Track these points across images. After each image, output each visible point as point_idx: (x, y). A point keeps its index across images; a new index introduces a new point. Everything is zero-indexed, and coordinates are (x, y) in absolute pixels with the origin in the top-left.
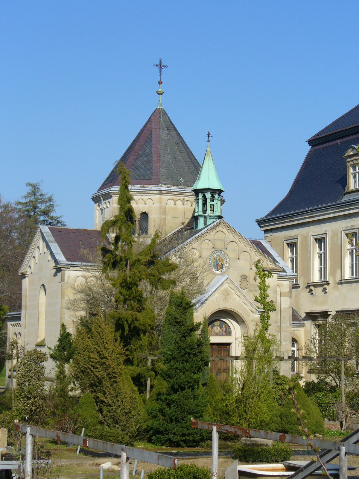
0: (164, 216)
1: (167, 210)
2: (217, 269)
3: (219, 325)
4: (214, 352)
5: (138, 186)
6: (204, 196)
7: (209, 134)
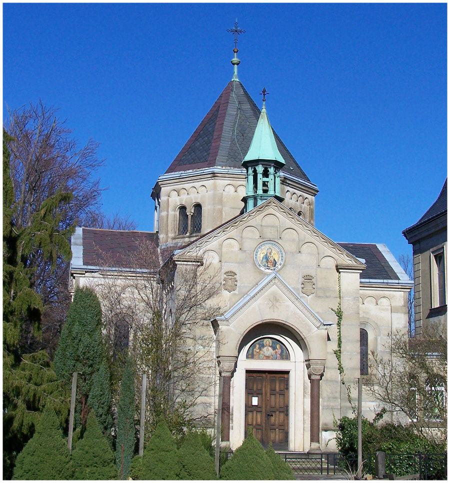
0: (220, 207)
1: (225, 200)
2: (268, 266)
3: (271, 345)
4: (264, 384)
5: (191, 171)
6: (255, 171)
7: (264, 91)
